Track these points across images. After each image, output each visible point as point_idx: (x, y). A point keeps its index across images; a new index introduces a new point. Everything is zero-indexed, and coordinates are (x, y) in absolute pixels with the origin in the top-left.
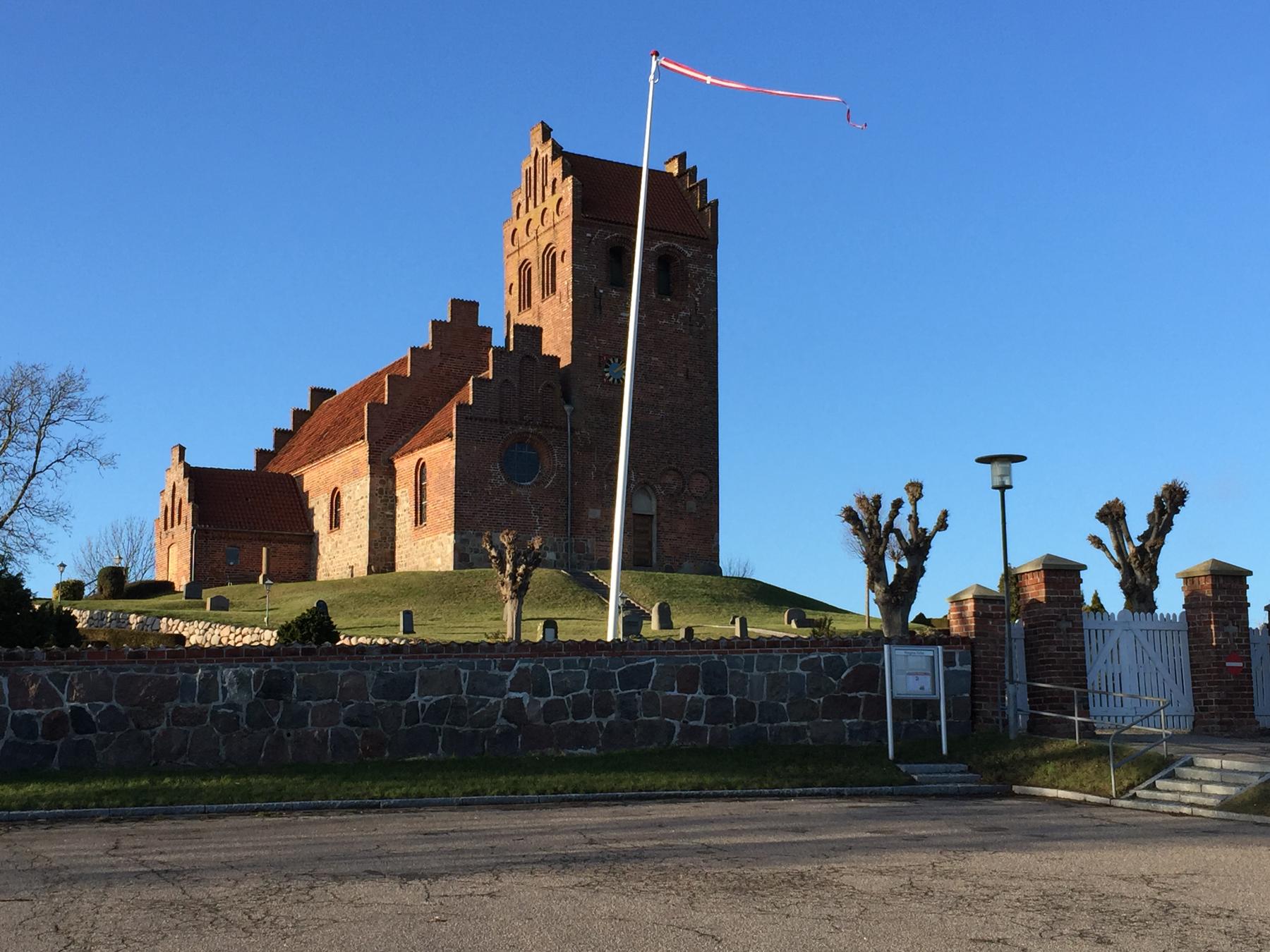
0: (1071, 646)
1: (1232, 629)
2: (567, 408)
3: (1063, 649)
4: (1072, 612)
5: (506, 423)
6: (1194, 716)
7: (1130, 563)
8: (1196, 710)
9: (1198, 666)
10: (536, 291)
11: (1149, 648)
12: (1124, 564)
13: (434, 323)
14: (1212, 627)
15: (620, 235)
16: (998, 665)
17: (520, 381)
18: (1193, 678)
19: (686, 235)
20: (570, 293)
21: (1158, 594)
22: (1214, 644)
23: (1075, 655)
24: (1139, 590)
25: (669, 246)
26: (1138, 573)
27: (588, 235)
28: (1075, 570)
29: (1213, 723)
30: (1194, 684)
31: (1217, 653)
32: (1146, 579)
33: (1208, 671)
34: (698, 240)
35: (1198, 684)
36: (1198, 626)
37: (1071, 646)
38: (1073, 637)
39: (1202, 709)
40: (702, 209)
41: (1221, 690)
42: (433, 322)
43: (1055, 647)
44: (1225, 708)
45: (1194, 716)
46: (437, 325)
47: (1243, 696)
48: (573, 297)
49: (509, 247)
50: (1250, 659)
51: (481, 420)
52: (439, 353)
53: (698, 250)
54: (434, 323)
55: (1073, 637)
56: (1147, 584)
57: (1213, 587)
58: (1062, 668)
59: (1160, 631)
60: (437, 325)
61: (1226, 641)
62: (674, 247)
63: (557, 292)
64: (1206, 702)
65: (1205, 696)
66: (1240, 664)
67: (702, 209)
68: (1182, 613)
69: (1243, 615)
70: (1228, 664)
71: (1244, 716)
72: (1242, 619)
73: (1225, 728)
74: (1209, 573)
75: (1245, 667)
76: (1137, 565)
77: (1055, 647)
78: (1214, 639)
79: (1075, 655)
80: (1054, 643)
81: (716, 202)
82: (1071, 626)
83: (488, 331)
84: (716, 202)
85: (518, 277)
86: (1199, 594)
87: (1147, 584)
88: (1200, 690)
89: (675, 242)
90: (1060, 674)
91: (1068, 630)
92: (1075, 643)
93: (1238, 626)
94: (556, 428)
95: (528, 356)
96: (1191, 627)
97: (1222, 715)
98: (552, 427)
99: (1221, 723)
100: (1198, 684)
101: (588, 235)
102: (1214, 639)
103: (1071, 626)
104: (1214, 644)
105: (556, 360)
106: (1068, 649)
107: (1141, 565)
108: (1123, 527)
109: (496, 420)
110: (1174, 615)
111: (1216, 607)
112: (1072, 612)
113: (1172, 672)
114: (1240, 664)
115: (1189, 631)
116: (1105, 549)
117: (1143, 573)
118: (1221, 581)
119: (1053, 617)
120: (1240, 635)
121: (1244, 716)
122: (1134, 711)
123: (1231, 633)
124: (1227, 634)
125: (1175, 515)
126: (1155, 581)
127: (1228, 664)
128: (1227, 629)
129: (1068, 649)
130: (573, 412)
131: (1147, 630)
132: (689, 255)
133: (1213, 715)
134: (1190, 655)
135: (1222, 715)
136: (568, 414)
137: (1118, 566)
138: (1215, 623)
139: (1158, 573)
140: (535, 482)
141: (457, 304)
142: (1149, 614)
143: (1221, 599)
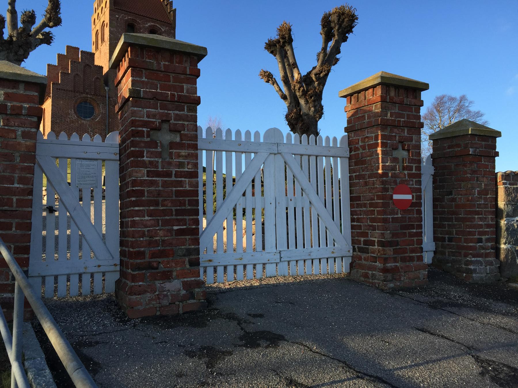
0: (174, 170)
1: (402, 154)
2: (106, 88)
3: (158, 174)
4: (178, 118)
5: (77, 92)
6: (352, 257)
7: (295, 90)
8: (354, 250)
9: (358, 198)
10: (100, 42)
11: (302, 178)
12: (290, 95)
13: (59, 55)
14: (379, 150)
15: (132, 18)
16: (15, 199)
17: (84, 75)
18: (352, 213)
19: (161, 21)
20: (109, 40)
21: (321, 124)
22: (380, 171)
23: (180, 184)
24: (302, 121)
25: (154, 25)
26: (302, 102)
27: (117, 16)
28: (188, 54)
29: (374, 268)
30: (353, 220)
31: (383, 183)
32: (310, 110)
33: (371, 205)
34: (167, 24)
35: (358, 220)
36: (361, 151)
37: (174, 170)
38: (179, 156)
39: (361, 250)
40: (170, 12)
41: (386, 229)
42: (58, 54)
43: (145, 171)
44: (390, 251)
45: (352, 257)
46: (60, 56)
47: (411, 235)
48: (109, 42)
49: (93, 26)
50: (419, 190)
51: (64, 90)
52: (61, 67)
53: (167, 28)
54: (59, 55)
55: (179, 156)
56: (311, 113)
57: (383, 100)
58: (157, 204)
59: (317, 156)
60: (60, 56)
61: (393, 169)
62: (156, 26)
63: (105, 41)
64: (366, 243)
65: (365, 235)
66: (409, 197)
67: (170, 12)
68: (343, 138)
69: (414, 137)
70: (396, 197)
71: (411, 259)
72: (414, 142)
73: (389, 276)
74: (379, 80)
75: (414, 201)
76: (301, 94)
77: (145, 171)
78: (381, 164)
79: (180, 184)
80: (144, 165)
81: (175, 10)
82: (178, 140)
83: (101, 68)
84: (175, 10)
85: (95, 38)
86: (365, 112)
87: (311, 113)
88: (360, 227)
89: (158, 24)
90: (150, 214)
91: (172, 145)
92: (181, 165)
93: (408, 150)
94: (101, 96)
95: (88, 65)
96: (353, 153)
97: (385, 260)
98: (99, 96)
99: (385, 270)
100: (358, 220)
101: (117, 16)
102: (381, 164)
103: (178, 140)
104: (380, 171)
105: (101, 68)
106: (169, 174)
107: (305, 93)
108: (289, 53)
109: (72, 91)
110: (335, 139)
111: (384, 125)
112: (178, 118)
113: (329, 204)
114: (409, 197)
115: (350, 158)
116: (275, 82)
117: (307, 102)
118: (392, 94)
119: (145, 124)
120: (411, 161)
121: (411, 259)
122: (278, 256)
123: (400, 159)
124: (395, 160)
125: (343, 43)
126: (319, 112)
127: (396, 197)
128: (395, 154)
129: (169, 174)
130: (109, 90)
131: (309, 156)
132: (163, 30)
133: (375, 260)
134: (351, 186)
135: (385, 260)
136: (107, 91)
137: (284, 97)
138: (384, 145)
139: (323, 102)
140: (92, 119)
141: (69, 48)
142: (304, 136)
143: (391, 116)
